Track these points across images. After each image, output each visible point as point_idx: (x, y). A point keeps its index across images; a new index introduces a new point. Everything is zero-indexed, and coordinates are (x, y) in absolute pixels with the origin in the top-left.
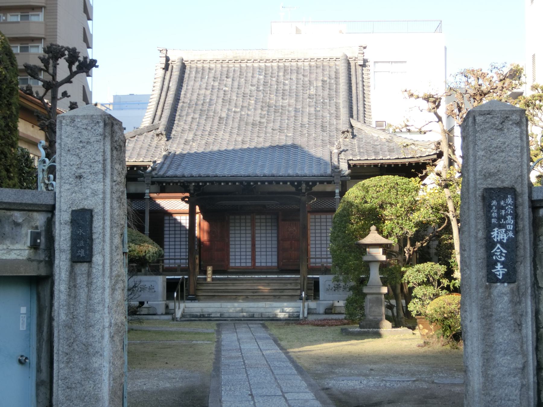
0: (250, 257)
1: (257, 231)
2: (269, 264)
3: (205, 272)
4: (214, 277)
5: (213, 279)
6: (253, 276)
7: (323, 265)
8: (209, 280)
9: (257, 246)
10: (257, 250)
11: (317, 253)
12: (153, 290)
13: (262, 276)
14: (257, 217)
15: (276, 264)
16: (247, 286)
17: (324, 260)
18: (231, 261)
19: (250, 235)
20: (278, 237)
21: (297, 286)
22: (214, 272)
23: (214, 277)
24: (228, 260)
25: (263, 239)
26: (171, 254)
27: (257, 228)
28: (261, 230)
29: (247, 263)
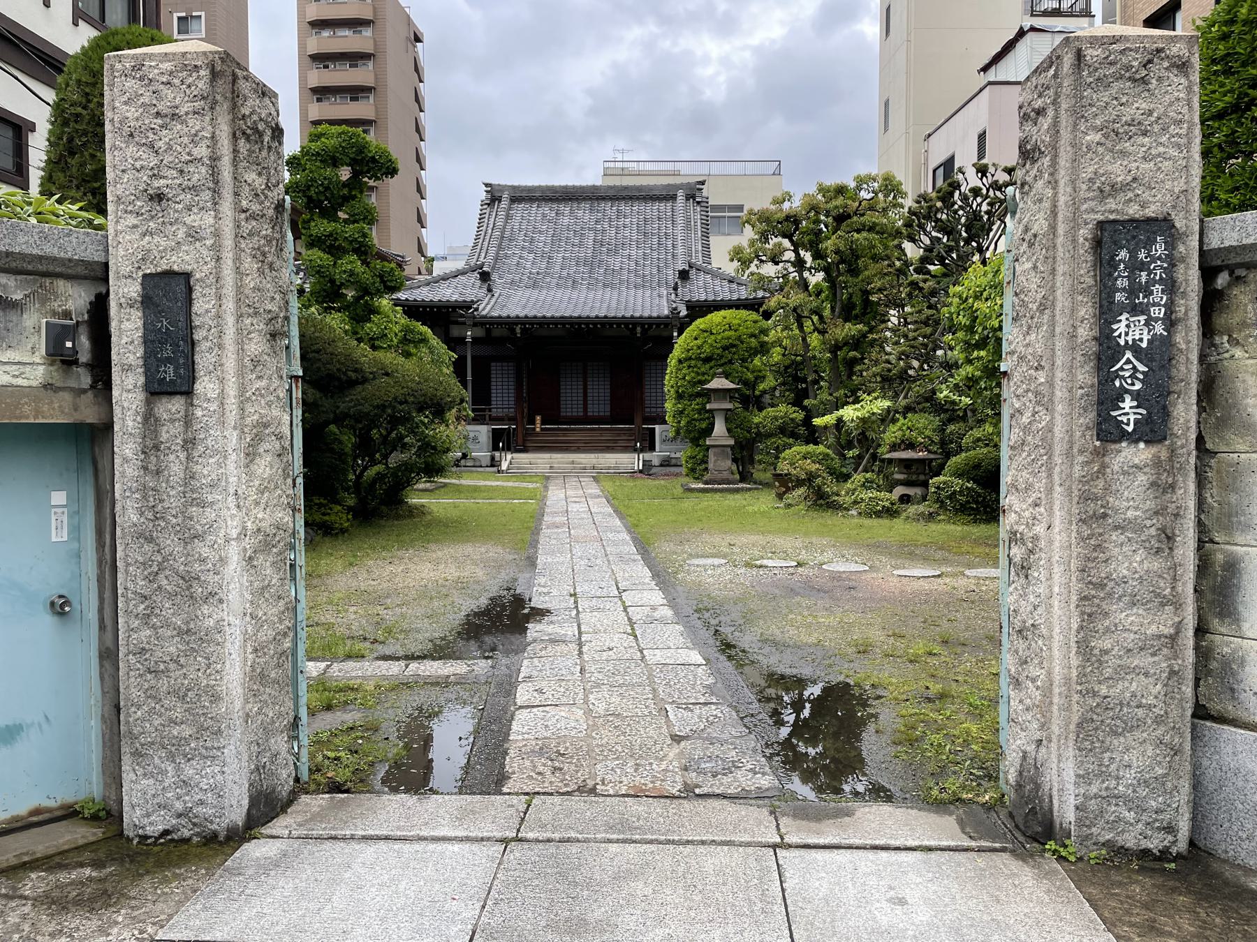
22: (543, 423)
24: (559, 408)
29: (578, 412)
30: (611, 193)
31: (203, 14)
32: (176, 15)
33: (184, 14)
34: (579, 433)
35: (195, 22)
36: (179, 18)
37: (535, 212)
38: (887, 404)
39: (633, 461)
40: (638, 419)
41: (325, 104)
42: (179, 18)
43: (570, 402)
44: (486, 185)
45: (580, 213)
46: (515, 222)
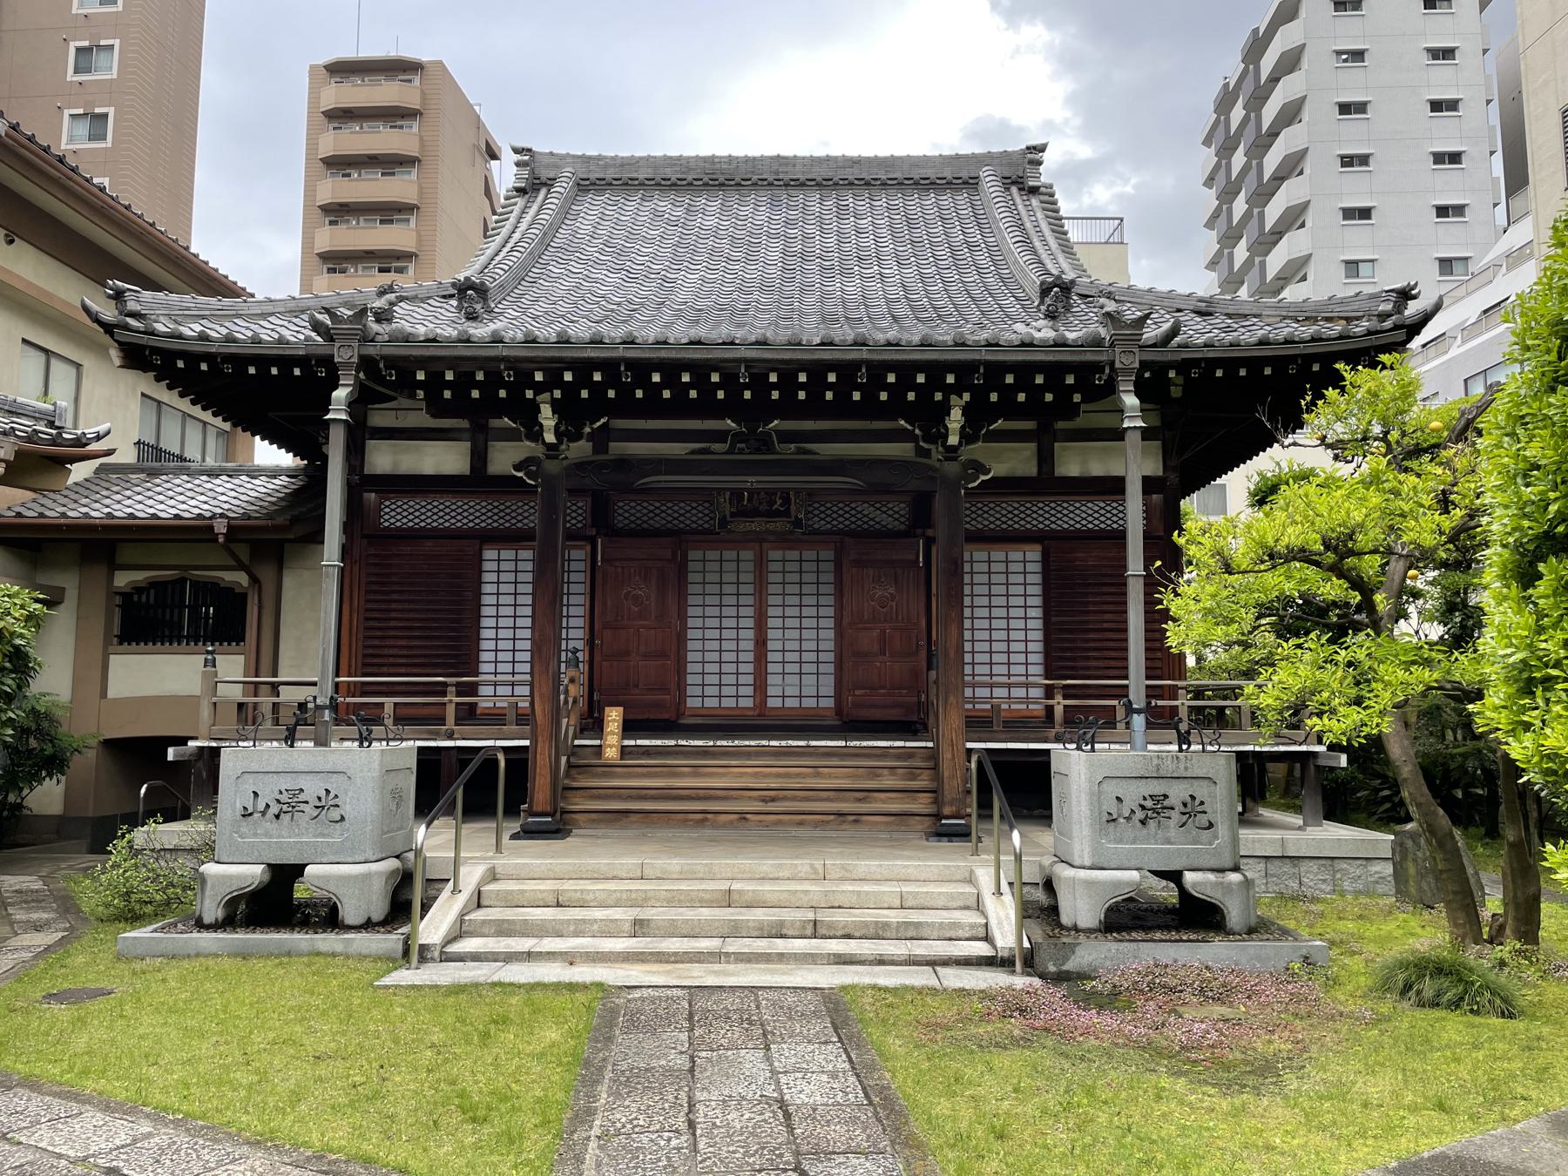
0: (750, 679)
1: (772, 600)
2: (809, 703)
3: (594, 724)
4: (626, 743)
5: (624, 752)
6: (764, 743)
7: (996, 708)
8: (611, 753)
9: (771, 645)
10: (771, 657)
11: (996, 669)
12: (335, 814)
13: (791, 743)
14: (775, 554)
15: (829, 703)
16: (742, 775)
17: (1000, 692)
18: (690, 691)
19: (750, 611)
20: (838, 619)
21: (914, 777)
22: (629, 728)
23: (626, 743)
24: (681, 686)
25: (789, 623)
26: (501, 668)
27: (772, 589)
28: (784, 594)
29: (738, 697)
30: (819, 173)
31: (117, 43)
32: (73, 45)
33: (86, 43)
34: (741, 769)
35: (103, 56)
36: (78, 50)
37: (633, 209)
38: (1470, 707)
39: (969, 893)
40: (950, 723)
41: (342, 227)
42: (78, 50)
43: (715, 666)
44: (516, 151)
45: (746, 210)
46: (584, 226)
